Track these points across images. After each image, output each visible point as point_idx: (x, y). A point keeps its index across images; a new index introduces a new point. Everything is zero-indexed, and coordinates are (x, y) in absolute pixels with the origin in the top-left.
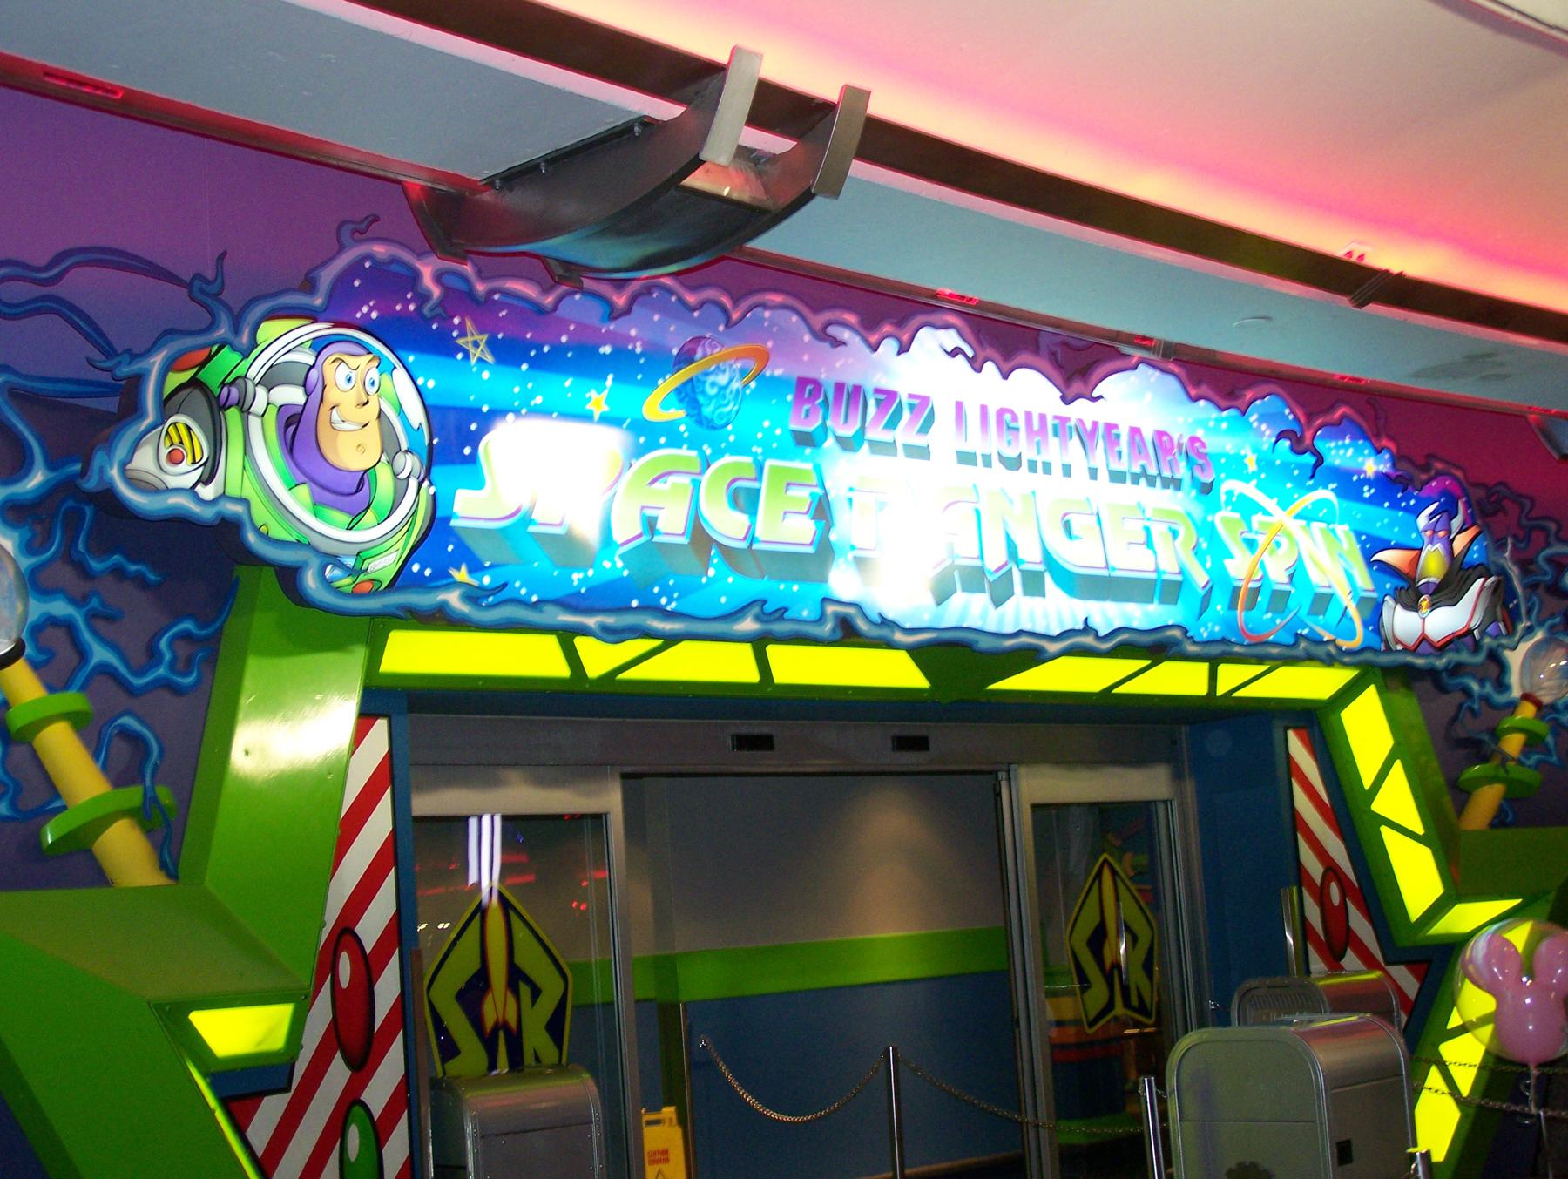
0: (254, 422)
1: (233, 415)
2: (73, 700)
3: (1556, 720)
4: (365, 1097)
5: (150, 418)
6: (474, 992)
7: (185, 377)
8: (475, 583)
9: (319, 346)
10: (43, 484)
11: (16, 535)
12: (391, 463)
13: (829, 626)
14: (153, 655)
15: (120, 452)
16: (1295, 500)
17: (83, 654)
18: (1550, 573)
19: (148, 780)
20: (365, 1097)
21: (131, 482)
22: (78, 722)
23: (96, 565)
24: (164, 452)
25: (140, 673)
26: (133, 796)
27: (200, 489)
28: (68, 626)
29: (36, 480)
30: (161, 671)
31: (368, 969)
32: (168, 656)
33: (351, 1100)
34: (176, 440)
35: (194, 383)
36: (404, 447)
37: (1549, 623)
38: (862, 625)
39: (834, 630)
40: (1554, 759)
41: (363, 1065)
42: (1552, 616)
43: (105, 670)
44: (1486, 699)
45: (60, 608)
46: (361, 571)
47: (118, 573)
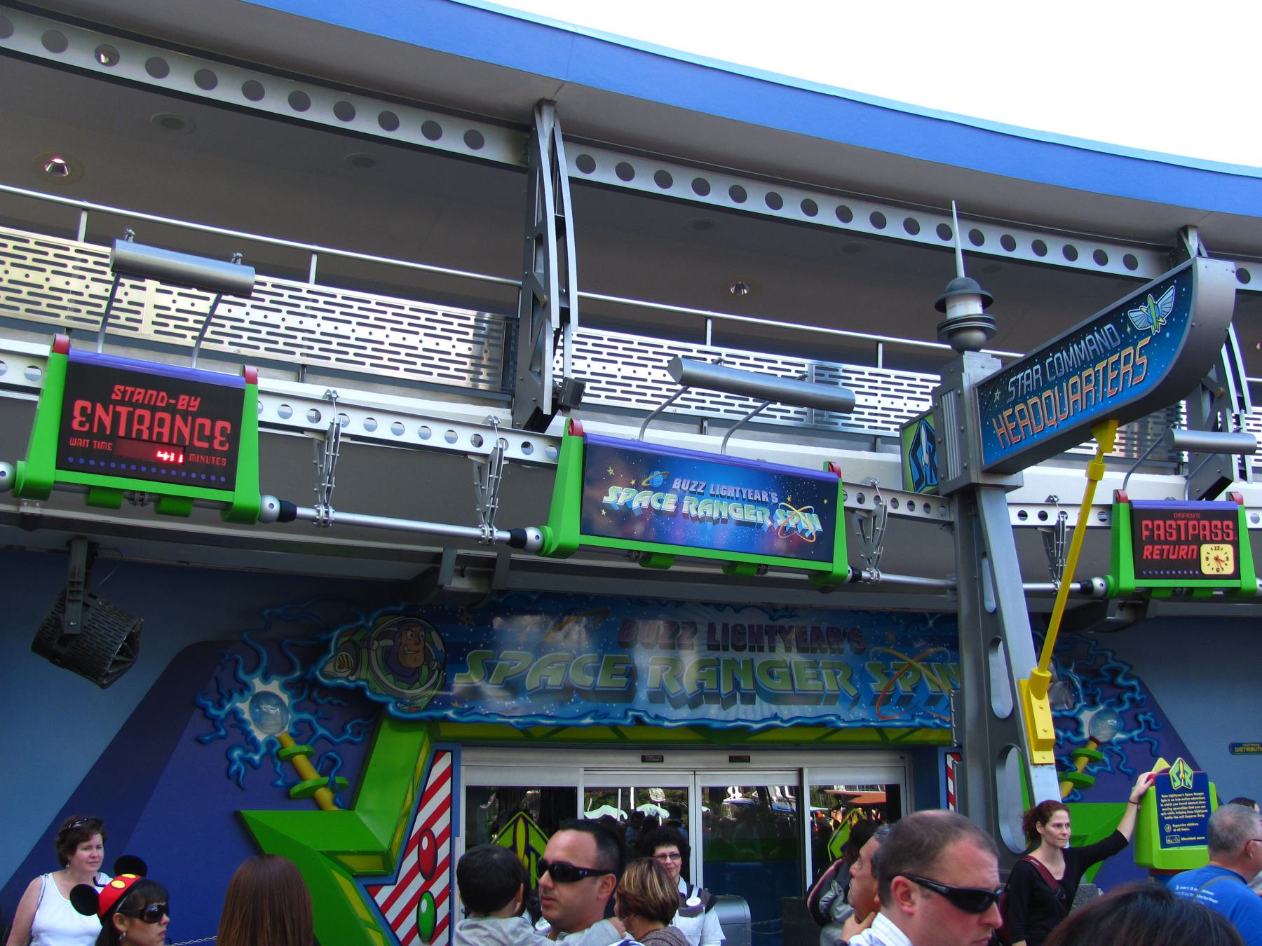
0: (373, 654)
1: (364, 652)
2: (305, 748)
3: (1111, 750)
4: (431, 890)
5: (332, 654)
6: (1178, 774)
7: (346, 639)
8: (461, 707)
9: (399, 625)
10: (299, 676)
11: (289, 693)
12: (428, 665)
13: (629, 721)
14: (343, 731)
15: (321, 665)
16: (904, 654)
17: (314, 731)
18: (1108, 676)
19: (332, 775)
20: (431, 890)
21: (323, 675)
22: (309, 756)
23: (320, 701)
24: (337, 665)
25: (337, 736)
26: (326, 779)
27: (350, 677)
28: (309, 723)
29: (297, 674)
30: (347, 737)
31: (436, 843)
32: (350, 731)
33: (424, 890)
34: (342, 660)
35: (350, 640)
36: (434, 658)
37: (1108, 701)
38: (646, 719)
39: (632, 722)
40: (1109, 769)
41: (431, 877)
42: (1110, 697)
43: (323, 737)
44: (1068, 740)
45: (306, 716)
46: (413, 704)
47: (330, 703)
